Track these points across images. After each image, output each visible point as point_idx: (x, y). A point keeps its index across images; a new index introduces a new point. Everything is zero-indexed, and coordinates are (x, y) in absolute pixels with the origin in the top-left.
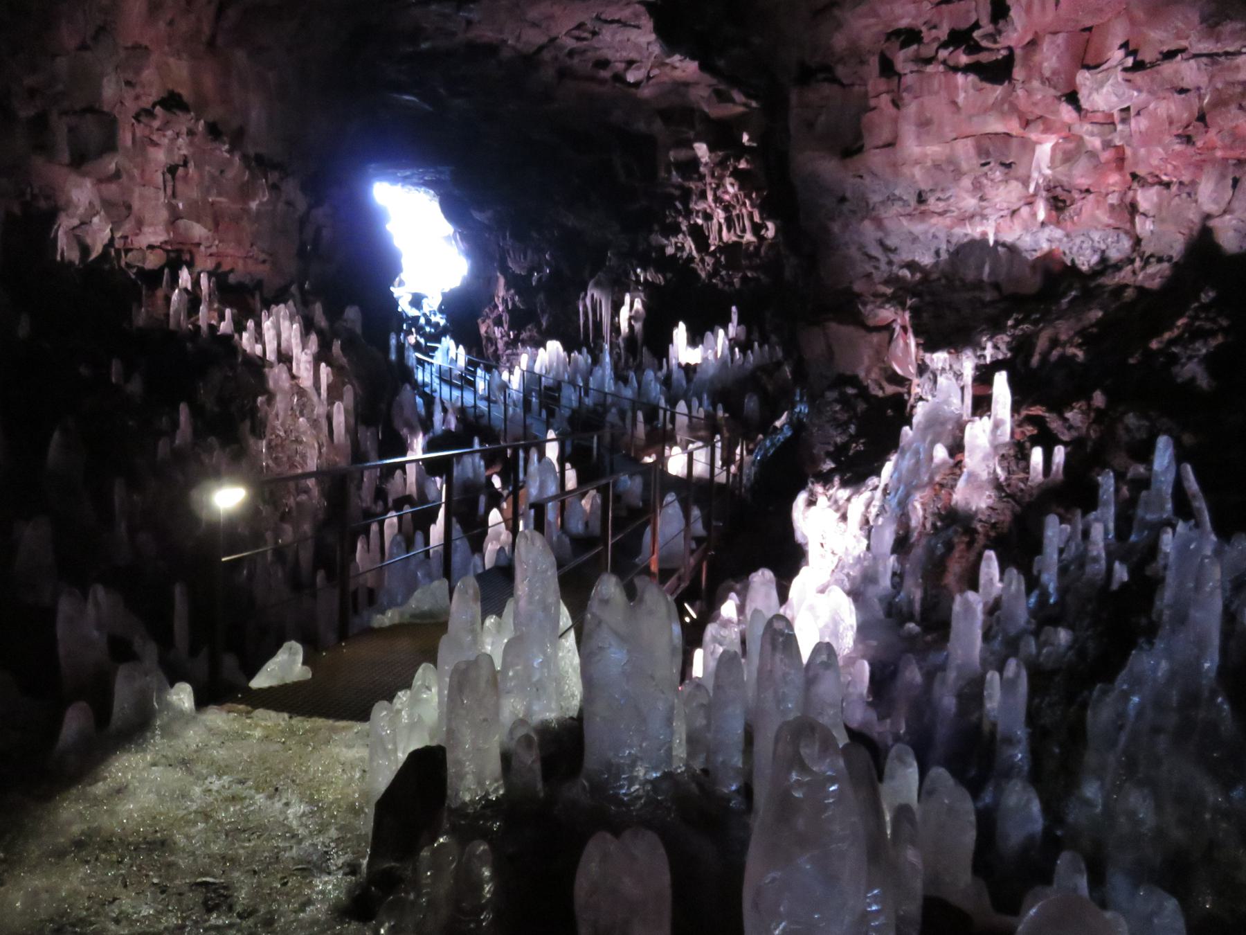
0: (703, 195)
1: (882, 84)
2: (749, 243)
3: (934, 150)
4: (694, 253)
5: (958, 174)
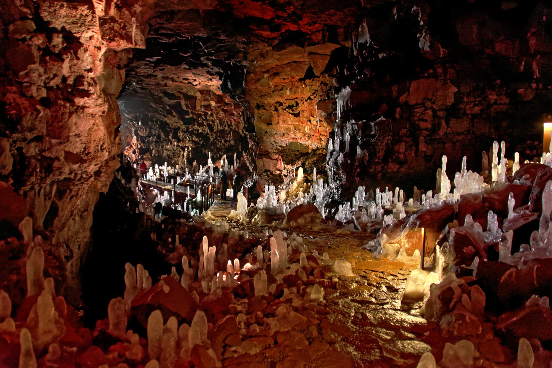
0: (212, 115)
1: (275, 112)
2: (227, 130)
3: (286, 126)
4: (209, 132)
5: (291, 131)
